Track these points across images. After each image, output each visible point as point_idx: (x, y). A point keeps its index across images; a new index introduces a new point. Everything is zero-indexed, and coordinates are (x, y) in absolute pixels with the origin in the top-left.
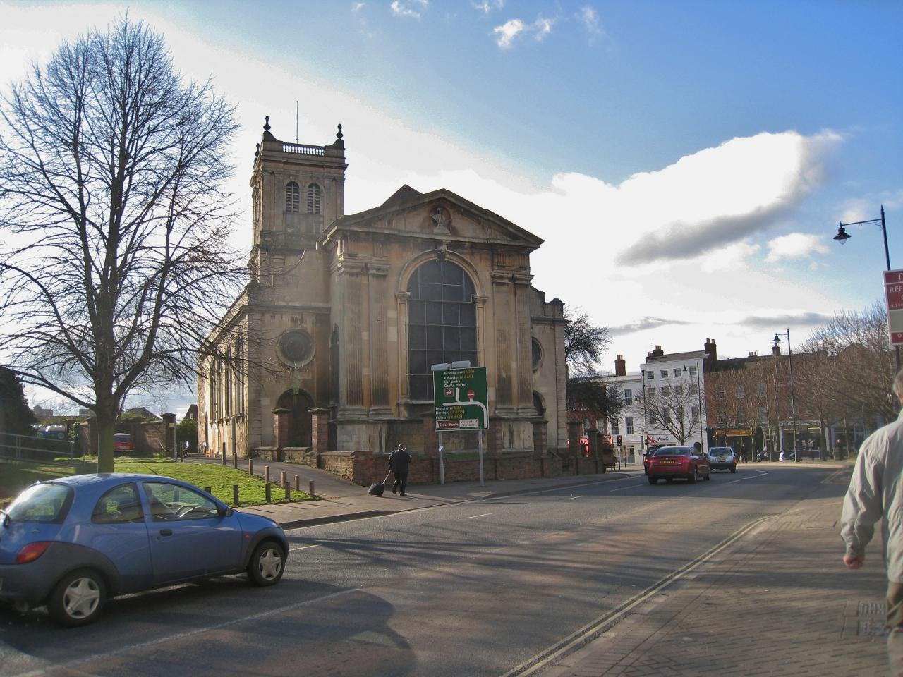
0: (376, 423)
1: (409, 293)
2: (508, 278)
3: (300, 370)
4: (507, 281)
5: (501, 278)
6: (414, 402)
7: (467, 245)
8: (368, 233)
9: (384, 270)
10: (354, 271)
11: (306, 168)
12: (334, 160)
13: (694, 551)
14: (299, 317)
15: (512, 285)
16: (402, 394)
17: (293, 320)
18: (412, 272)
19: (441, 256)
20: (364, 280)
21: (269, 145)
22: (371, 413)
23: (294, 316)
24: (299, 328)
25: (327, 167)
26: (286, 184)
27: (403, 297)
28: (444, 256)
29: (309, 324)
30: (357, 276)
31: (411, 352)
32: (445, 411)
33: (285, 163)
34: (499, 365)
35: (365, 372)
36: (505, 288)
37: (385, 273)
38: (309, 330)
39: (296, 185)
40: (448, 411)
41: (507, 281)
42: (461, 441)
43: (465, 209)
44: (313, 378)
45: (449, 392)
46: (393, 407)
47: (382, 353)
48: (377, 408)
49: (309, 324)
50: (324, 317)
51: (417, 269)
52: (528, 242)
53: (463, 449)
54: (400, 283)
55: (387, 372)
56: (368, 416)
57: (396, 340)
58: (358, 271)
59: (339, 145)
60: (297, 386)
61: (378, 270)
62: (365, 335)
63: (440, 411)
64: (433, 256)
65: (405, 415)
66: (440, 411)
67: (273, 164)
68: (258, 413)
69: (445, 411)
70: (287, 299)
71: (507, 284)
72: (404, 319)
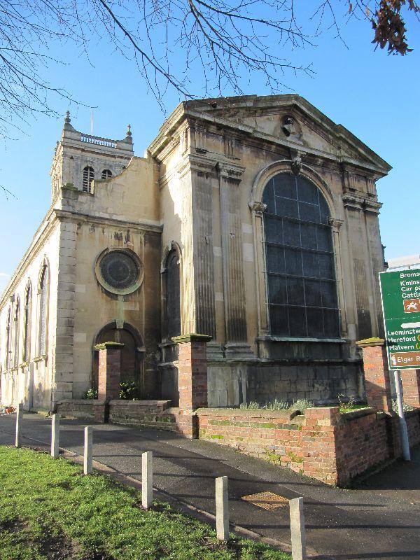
0: (234, 365)
1: (265, 206)
2: (359, 203)
3: (126, 297)
4: (358, 206)
5: (353, 202)
6: (276, 339)
7: (320, 161)
8: (220, 127)
9: (237, 174)
10: (203, 169)
11: (101, 157)
12: (125, 152)
13: (366, 468)
14: (124, 235)
15: (362, 213)
16: (262, 329)
17: (118, 237)
18: (266, 182)
19: (295, 168)
20: (214, 183)
21: (68, 134)
22: (227, 351)
23: (119, 233)
24: (124, 246)
25: (118, 157)
26: (83, 167)
27: (259, 209)
28: (299, 169)
29: (137, 244)
30: (207, 178)
31: (271, 277)
32: (408, 336)
33: (83, 150)
34: (358, 300)
35: (218, 297)
36: (357, 213)
37: (239, 178)
38: (136, 251)
39: (92, 169)
40: (412, 336)
41: (358, 206)
42: (326, 389)
43: (316, 123)
44: (141, 310)
45: (412, 305)
46: (251, 343)
47: (237, 274)
48: (234, 345)
49: (137, 244)
50: (154, 236)
51: (271, 179)
52: (384, 168)
53: (329, 399)
54: (253, 193)
55: (243, 298)
56: (224, 357)
57: (252, 260)
58: (208, 170)
59: (129, 140)
60: (121, 320)
61: (231, 172)
62: (217, 251)
63: (395, 337)
64: (288, 167)
65: (265, 354)
66: (395, 337)
67: (72, 150)
68: (70, 352)
69: (408, 336)
70: (110, 210)
71: (359, 210)
72: (260, 236)
